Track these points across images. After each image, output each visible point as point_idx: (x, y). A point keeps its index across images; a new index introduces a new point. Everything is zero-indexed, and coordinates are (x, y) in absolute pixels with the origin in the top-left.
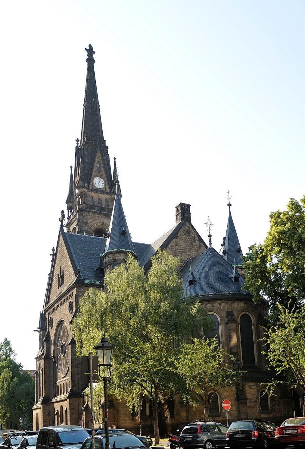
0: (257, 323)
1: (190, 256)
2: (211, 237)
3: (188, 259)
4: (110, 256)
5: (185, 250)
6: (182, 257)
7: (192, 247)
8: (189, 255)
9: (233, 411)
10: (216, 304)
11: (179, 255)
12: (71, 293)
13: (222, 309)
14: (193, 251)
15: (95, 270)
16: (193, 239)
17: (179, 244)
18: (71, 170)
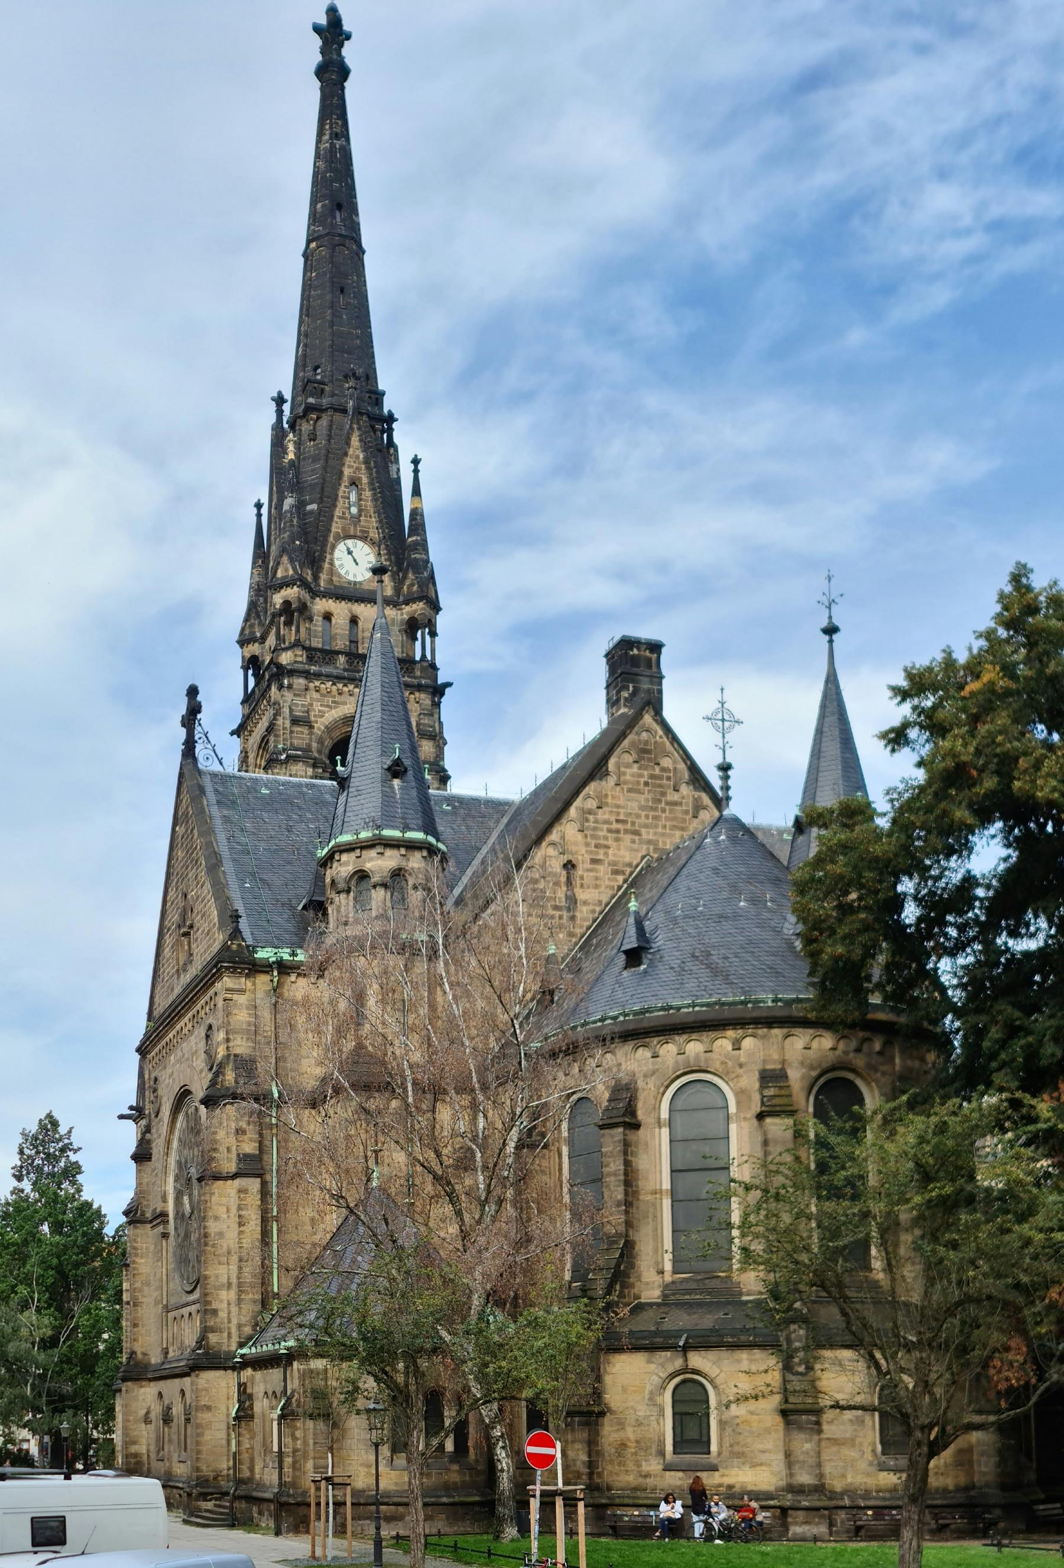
1: (651, 848)
2: (730, 773)
3: (643, 857)
4: (345, 857)
5: (633, 823)
7: (664, 811)
8: (649, 842)
9: (763, 1452)
10: (719, 1042)
11: (610, 842)
12: (211, 992)
13: (742, 1060)
14: (665, 827)
15: (300, 907)
16: (669, 778)
17: (609, 800)
18: (259, 515)
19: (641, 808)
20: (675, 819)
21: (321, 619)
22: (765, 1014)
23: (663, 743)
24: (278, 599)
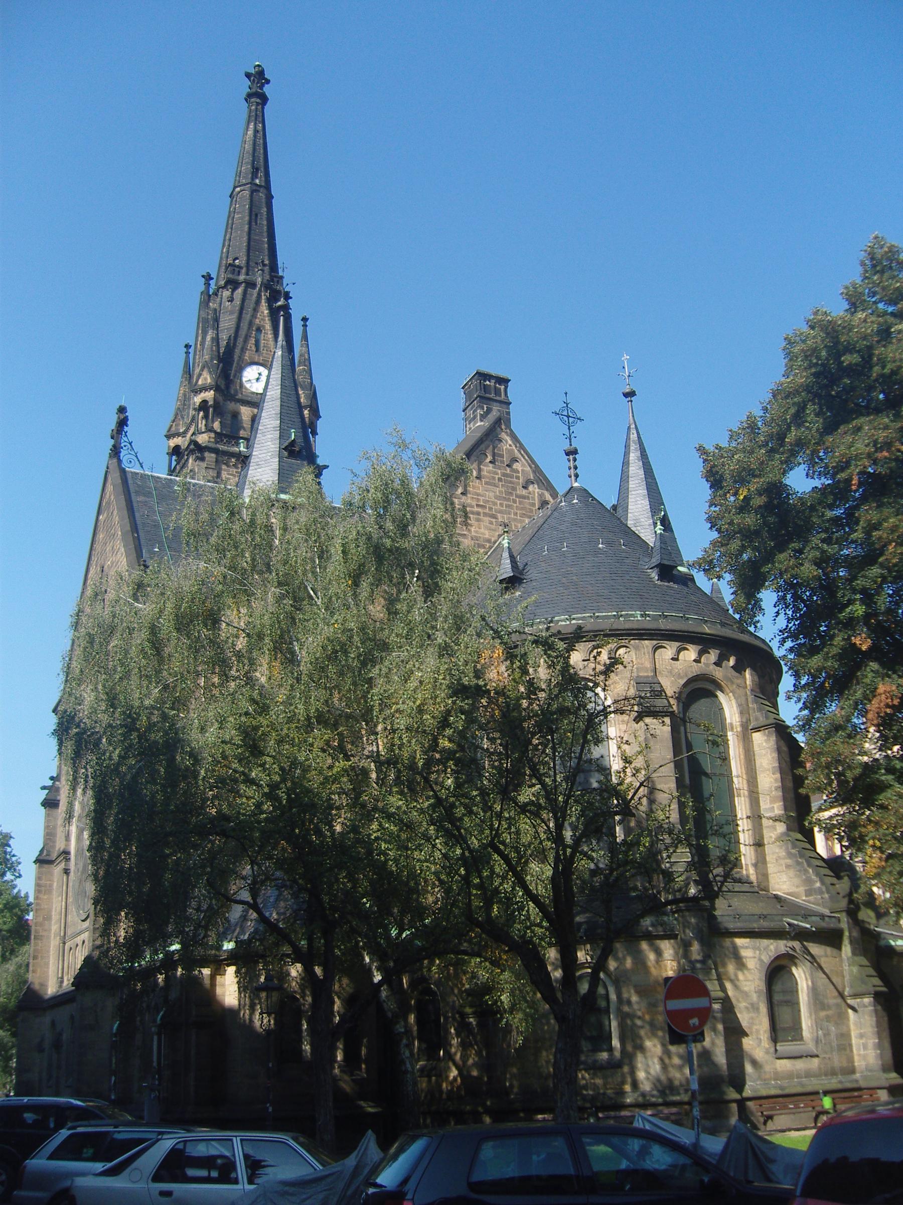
0: (744, 720)
5: (491, 509)
6: (482, 530)
7: (515, 502)
14: (516, 514)
19: (496, 497)
20: (522, 509)
21: (229, 415)
22: (635, 626)
23: (513, 450)
24: (198, 399)
